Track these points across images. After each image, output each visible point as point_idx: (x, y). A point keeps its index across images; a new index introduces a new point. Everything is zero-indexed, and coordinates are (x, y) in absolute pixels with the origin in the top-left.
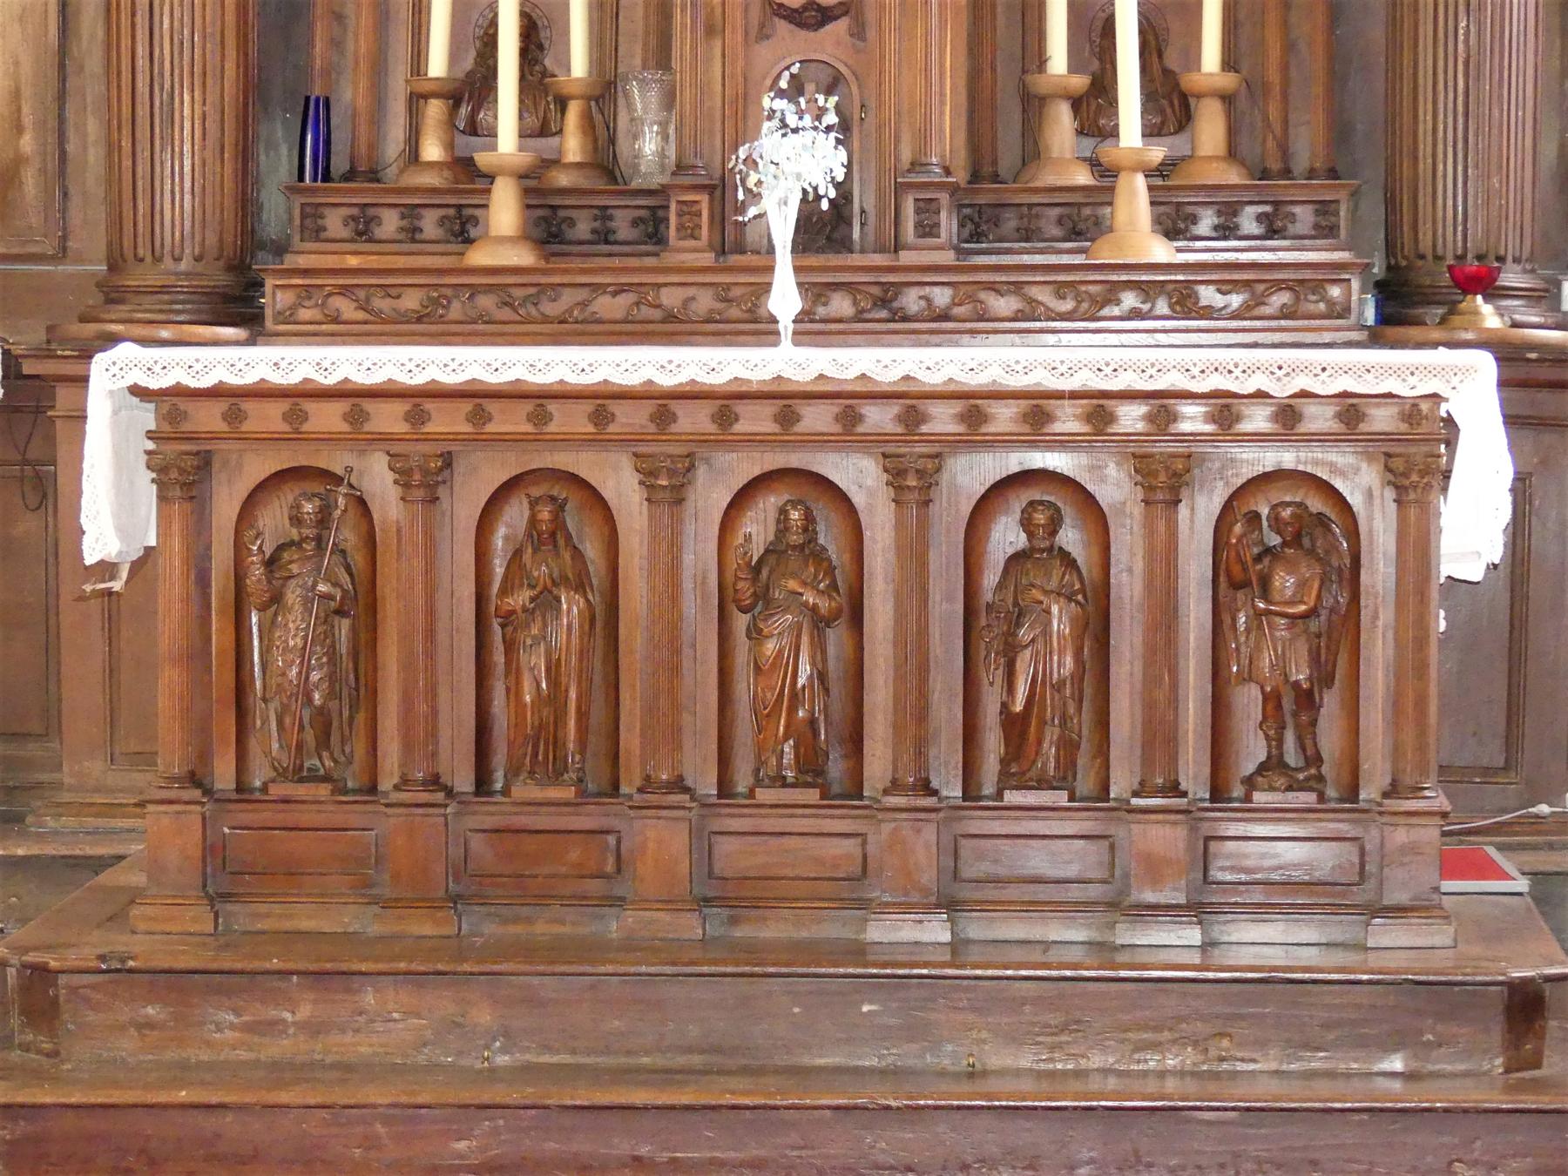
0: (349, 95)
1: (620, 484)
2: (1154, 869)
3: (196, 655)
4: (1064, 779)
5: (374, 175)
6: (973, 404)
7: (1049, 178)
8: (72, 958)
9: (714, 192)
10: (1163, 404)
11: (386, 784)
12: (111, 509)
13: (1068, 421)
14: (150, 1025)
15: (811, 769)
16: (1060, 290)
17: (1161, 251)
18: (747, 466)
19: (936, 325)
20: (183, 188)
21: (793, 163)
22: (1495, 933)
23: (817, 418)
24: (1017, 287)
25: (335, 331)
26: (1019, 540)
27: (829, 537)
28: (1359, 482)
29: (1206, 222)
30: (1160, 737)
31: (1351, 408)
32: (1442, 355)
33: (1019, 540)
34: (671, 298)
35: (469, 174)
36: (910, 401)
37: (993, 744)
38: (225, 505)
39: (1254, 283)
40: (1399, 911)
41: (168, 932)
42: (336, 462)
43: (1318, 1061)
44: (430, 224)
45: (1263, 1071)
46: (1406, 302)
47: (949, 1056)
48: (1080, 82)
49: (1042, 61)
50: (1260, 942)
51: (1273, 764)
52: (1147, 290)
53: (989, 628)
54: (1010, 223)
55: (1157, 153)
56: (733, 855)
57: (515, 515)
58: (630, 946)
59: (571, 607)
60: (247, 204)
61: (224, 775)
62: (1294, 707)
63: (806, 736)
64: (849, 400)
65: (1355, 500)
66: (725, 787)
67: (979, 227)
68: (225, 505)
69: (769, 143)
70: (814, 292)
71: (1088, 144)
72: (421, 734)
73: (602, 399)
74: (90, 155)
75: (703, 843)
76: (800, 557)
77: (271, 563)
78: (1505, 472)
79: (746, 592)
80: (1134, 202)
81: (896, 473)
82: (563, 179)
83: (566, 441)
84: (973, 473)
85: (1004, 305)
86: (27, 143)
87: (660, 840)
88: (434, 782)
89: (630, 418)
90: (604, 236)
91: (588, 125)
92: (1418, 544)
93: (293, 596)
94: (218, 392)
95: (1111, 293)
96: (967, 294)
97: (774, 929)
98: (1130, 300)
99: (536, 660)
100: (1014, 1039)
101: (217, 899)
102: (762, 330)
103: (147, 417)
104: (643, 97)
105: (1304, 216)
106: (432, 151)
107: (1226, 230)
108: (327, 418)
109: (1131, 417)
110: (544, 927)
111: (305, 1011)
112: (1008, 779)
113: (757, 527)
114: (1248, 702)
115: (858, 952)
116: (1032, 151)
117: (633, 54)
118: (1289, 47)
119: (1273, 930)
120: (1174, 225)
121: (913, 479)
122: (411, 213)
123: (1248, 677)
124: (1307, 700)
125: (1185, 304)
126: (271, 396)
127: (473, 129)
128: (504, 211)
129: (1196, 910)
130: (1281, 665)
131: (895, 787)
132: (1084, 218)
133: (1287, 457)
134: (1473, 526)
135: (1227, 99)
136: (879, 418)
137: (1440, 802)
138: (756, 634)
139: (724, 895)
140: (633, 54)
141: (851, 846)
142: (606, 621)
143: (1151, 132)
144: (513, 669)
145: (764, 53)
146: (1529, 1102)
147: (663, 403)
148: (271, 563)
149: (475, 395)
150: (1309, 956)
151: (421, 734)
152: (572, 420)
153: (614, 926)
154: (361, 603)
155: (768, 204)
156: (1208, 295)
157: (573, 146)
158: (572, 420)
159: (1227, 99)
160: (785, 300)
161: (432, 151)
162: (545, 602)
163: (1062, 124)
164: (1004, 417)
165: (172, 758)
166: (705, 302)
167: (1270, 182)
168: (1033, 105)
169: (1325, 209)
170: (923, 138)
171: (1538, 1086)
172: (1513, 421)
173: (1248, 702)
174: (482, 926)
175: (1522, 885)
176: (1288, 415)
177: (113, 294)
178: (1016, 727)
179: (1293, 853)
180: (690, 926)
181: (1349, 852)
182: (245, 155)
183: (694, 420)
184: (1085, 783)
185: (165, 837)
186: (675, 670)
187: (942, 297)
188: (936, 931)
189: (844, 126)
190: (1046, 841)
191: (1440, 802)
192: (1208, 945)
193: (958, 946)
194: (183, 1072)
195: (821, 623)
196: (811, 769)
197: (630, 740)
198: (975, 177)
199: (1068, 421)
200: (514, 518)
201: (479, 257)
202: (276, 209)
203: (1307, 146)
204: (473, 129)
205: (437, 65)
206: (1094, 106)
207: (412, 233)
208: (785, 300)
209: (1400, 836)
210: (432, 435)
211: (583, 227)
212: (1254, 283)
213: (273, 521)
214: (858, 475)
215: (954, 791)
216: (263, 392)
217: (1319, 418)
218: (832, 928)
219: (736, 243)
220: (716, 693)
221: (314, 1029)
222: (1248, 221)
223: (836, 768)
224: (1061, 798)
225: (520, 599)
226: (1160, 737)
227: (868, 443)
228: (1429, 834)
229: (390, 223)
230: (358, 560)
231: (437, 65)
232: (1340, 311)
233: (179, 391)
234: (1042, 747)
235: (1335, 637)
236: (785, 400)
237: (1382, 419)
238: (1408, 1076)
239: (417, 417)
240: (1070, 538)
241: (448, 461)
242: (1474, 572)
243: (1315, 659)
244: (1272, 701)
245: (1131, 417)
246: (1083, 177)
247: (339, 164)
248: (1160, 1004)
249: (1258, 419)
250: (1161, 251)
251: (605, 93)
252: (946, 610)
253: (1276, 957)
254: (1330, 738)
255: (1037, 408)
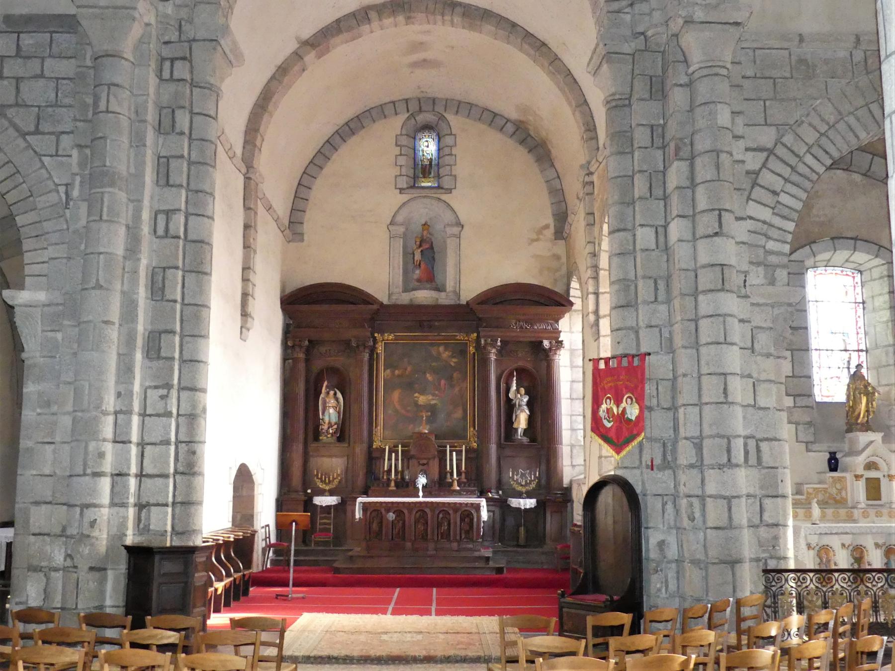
1: (406, 511)
12: (358, 515)
20: (360, 481)
21: (422, 481)
30: (455, 535)
35: (389, 480)
53: (439, 525)
68: (369, 513)
80: (456, 483)
92: (479, 517)
102: (418, 497)
113: (418, 515)
116: (445, 478)
128: (393, 484)
132: (451, 484)
160: (421, 494)
168: (446, 473)
208: (421, 494)
210: (389, 507)
220: (368, 616)
226: (455, 535)
251: (403, 472)
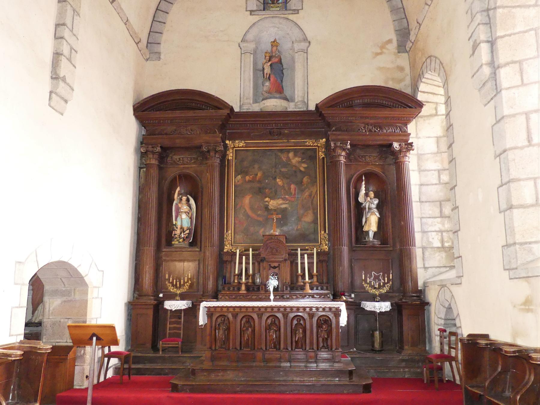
0: (228, 275)
1: (255, 316)
2: (311, 357)
3: (210, 335)
4: (301, 348)
5: (230, 284)
6: (291, 308)
7: (299, 284)
8: (197, 368)
9: (264, 286)
10: (311, 308)
11: (231, 348)
13: (301, 310)
14: (205, 375)
15: (275, 347)
16: (300, 296)
17: (310, 291)
18: (268, 315)
19: (288, 299)
20: (210, 284)
21: (273, 283)
22: (347, 364)
23: (275, 310)
24: (296, 295)
25: (226, 300)
26: (296, 322)
27: (277, 322)
28: (331, 316)
29: (315, 288)
30: (311, 343)
31: (330, 309)
32: (339, 303)
33: (296, 322)
34: (260, 296)
35: (240, 284)
36: (285, 308)
37: (294, 344)
38: (214, 319)
39: (320, 295)
40: (337, 362)
41: (207, 365)
42: (226, 314)
43: (329, 379)
44: (236, 289)
45: (323, 380)
46: (336, 297)
47: (290, 379)
48: (302, 274)
49: (298, 272)
50: (323, 366)
51: (323, 346)
52: (309, 296)
53: (293, 332)
54: (295, 288)
55: (310, 281)
56: (267, 356)
57: (244, 320)
58: (256, 366)
59: (250, 330)
60: (217, 286)
61: (213, 348)
62: (325, 340)
63: (275, 343)
64: (279, 308)
65: (331, 318)
66: (266, 349)
67: (292, 289)
68: (214, 319)
69: (270, 281)
70: (275, 296)
71: (303, 281)
72: (234, 344)
73: (253, 308)
74: (201, 281)
75: (264, 355)
76: (274, 323)
77: (219, 325)
78: (346, 315)
79: (268, 328)
80: (308, 286)
81: (284, 315)
82: (249, 284)
83: (249, 312)
84: (292, 315)
85: (295, 297)
86: (195, 280)
87: (259, 355)
88: (236, 348)
89: (257, 310)
90: (253, 290)
91: (252, 278)
92: (338, 322)
93: (221, 328)
94: (214, 307)
95: (305, 296)
96: (291, 296)
97: (271, 364)
98: (307, 297)
99: (246, 335)
100: (297, 377)
101: (212, 361)
102: (269, 300)
103: (206, 309)
104: (367, 189)
105: (325, 288)
106: (236, 281)
107: (317, 289)
108: (225, 310)
109: (308, 309)
110: (247, 364)
111: (222, 374)
112: (296, 348)
113: (269, 321)
114: (321, 339)
115: (280, 367)
116: (297, 281)
117: (256, 271)
118: (323, 270)
119: (323, 364)
120: (312, 289)
121: (285, 316)
122: (234, 287)
123: (320, 337)
124: (327, 339)
125: (313, 297)
126: (492, 52)
127: (240, 279)
128: (243, 287)
129: (316, 362)
130: (324, 336)
131: (284, 349)
132: (303, 288)
133: (324, 313)
134: (343, 320)
135: (317, 276)
136: (282, 309)
137: (341, 350)
138: (269, 332)
139: (267, 361)
140: (256, 271)
141: (279, 355)
142: (253, 331)
143: (309, 279)
144: (244, 337)
145: (270, 271)
146: (352, 383)
147: (259, 308)
148: (219, 325)
149: (240, 307)
150: (328, 367)
151: (234, 344)
152: (250, 310)
153: (254, 364)
154: (228, 329)
155: (270, 287)
156: (315, 296)
157: (250, 281)
158: (250, 310)
159: (317, 276)
160: (272, 297)
161: (236, 281)
162: (247, 329)
163: (300, 278)
164: (295, 309)
165: (208, 345)
166: (264, 297)
167: (321, 284)
168: (297, 276)
169: (327, 287)
170: (286, 280)
171: (353, 381)
172: (347, 309)
173: (321, 339)
174: (240, 364)
175: (350, 359)
176: (324, 309)
177: (203, 295)
178: (297, 342)
179: (325, 356)
180: (262, 364)
181: (331, 356)
182: (217, 281)
183: (263, 310)
184: (304, 348)
185: (206, 354)
186: (261, 336)
187: (288, 296)
188: (288, 364)
189: (278, 279)
190: (300, 354)
191: (341, 350)
192: (317, 366)
193: (290, 366)
194: (209, 381)
195: (276, 331)
196: (275, 347)
197: (256, 344)
198: (291, 284)
199: (301, 310)
200: (244, 320)
201: (241, 292)
202: (220, 287)
203: (325, 281)
204: (240, 279)
205: (237, 272)
206: (303, 276)
207: (234, 289)
208: (272, 297)
209: (337, 354)
210: (236, 311)
211: (251, 289)
212: (320, 295)
213: (219, 320)
214: (280, 315)
215: (290, 349)
216: (218, 307)
217: (327, 309)
218: (278, 364)
219: (267, 291)
221: (223, 376)
222: (319, 288)
223: (278, 347)
224: (301, 350)
225: (245, 329)
226: (311, 343)
227: (281, 312)
228: (340, 354)
229: (232, 289)
230: (228, 324)
231: (237, 272)
232: (329, 298)
233: (210, 307)
234: (300, 344)
235: (329, 333)
236: (272, 308)
237: (334, 310)
238: (339, 381)
239: (234, 309)
240: (302, 322)
241: (237, 314)
242: (343, 325)
243: (327, 335)
244: (323, 339)
245: (308, 309)
246: (302, 284)
247: (226, 282)
248: (312, 373)
249: (321, 310)
250: (310, 291)
251: (254, 275)
252: (289, 329)
253: (324, 367)
254: (329, 343)
255: (298, 309)
